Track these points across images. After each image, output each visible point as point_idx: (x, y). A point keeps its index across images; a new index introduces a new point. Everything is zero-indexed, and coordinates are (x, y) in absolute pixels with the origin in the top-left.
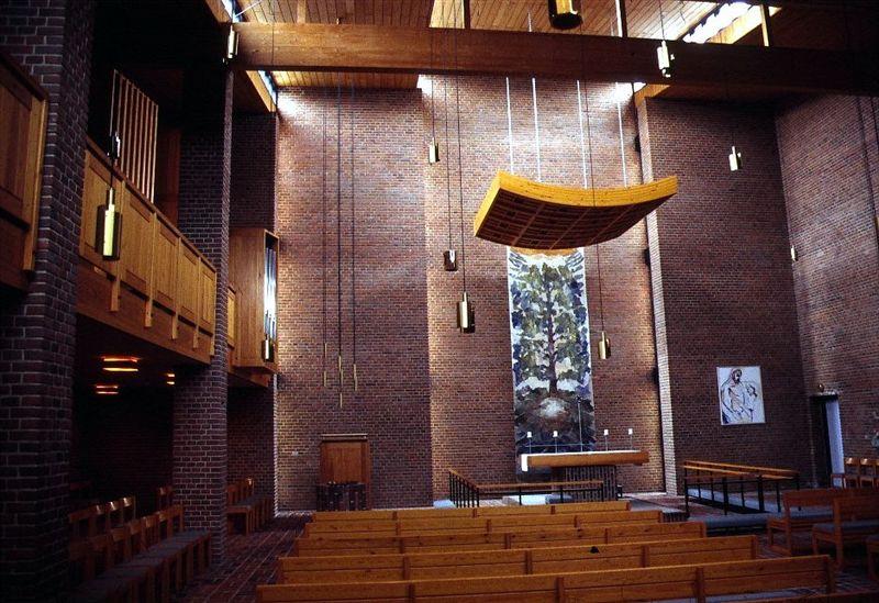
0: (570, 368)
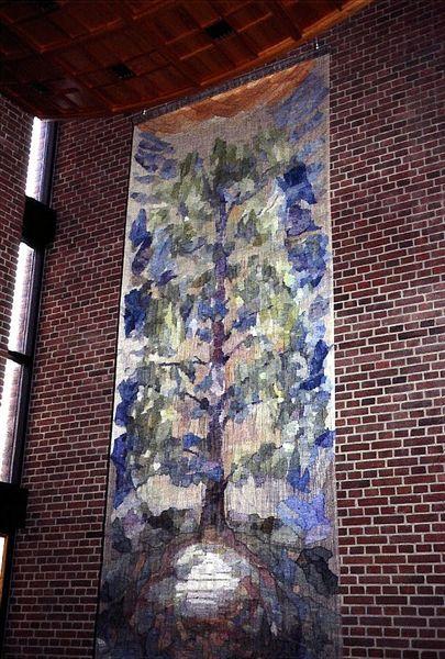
0: (268, 438)
